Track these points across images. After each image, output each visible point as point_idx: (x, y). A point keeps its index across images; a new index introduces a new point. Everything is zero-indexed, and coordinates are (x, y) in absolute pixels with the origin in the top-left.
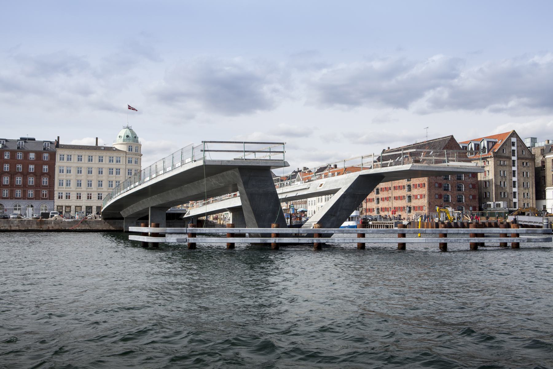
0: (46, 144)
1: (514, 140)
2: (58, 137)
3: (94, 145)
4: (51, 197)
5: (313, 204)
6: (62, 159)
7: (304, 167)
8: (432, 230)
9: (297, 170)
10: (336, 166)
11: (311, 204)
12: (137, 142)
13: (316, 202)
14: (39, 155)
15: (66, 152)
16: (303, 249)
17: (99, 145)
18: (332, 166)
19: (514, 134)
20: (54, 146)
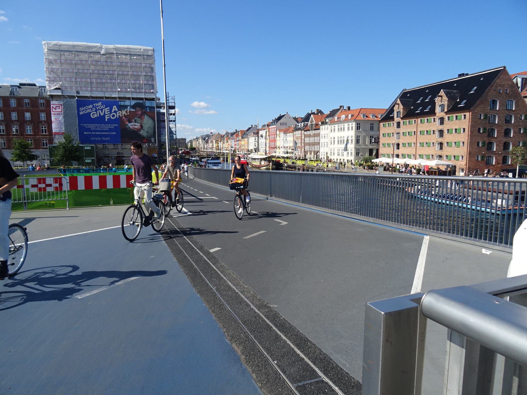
0: (42, 89)
5: (326, 146)
7: (317, 110)
8: (56, 194)
9: (310, 112)
10: (349, 108)
11: (323, 145)
13: (328, 144)
18: (345, 108)
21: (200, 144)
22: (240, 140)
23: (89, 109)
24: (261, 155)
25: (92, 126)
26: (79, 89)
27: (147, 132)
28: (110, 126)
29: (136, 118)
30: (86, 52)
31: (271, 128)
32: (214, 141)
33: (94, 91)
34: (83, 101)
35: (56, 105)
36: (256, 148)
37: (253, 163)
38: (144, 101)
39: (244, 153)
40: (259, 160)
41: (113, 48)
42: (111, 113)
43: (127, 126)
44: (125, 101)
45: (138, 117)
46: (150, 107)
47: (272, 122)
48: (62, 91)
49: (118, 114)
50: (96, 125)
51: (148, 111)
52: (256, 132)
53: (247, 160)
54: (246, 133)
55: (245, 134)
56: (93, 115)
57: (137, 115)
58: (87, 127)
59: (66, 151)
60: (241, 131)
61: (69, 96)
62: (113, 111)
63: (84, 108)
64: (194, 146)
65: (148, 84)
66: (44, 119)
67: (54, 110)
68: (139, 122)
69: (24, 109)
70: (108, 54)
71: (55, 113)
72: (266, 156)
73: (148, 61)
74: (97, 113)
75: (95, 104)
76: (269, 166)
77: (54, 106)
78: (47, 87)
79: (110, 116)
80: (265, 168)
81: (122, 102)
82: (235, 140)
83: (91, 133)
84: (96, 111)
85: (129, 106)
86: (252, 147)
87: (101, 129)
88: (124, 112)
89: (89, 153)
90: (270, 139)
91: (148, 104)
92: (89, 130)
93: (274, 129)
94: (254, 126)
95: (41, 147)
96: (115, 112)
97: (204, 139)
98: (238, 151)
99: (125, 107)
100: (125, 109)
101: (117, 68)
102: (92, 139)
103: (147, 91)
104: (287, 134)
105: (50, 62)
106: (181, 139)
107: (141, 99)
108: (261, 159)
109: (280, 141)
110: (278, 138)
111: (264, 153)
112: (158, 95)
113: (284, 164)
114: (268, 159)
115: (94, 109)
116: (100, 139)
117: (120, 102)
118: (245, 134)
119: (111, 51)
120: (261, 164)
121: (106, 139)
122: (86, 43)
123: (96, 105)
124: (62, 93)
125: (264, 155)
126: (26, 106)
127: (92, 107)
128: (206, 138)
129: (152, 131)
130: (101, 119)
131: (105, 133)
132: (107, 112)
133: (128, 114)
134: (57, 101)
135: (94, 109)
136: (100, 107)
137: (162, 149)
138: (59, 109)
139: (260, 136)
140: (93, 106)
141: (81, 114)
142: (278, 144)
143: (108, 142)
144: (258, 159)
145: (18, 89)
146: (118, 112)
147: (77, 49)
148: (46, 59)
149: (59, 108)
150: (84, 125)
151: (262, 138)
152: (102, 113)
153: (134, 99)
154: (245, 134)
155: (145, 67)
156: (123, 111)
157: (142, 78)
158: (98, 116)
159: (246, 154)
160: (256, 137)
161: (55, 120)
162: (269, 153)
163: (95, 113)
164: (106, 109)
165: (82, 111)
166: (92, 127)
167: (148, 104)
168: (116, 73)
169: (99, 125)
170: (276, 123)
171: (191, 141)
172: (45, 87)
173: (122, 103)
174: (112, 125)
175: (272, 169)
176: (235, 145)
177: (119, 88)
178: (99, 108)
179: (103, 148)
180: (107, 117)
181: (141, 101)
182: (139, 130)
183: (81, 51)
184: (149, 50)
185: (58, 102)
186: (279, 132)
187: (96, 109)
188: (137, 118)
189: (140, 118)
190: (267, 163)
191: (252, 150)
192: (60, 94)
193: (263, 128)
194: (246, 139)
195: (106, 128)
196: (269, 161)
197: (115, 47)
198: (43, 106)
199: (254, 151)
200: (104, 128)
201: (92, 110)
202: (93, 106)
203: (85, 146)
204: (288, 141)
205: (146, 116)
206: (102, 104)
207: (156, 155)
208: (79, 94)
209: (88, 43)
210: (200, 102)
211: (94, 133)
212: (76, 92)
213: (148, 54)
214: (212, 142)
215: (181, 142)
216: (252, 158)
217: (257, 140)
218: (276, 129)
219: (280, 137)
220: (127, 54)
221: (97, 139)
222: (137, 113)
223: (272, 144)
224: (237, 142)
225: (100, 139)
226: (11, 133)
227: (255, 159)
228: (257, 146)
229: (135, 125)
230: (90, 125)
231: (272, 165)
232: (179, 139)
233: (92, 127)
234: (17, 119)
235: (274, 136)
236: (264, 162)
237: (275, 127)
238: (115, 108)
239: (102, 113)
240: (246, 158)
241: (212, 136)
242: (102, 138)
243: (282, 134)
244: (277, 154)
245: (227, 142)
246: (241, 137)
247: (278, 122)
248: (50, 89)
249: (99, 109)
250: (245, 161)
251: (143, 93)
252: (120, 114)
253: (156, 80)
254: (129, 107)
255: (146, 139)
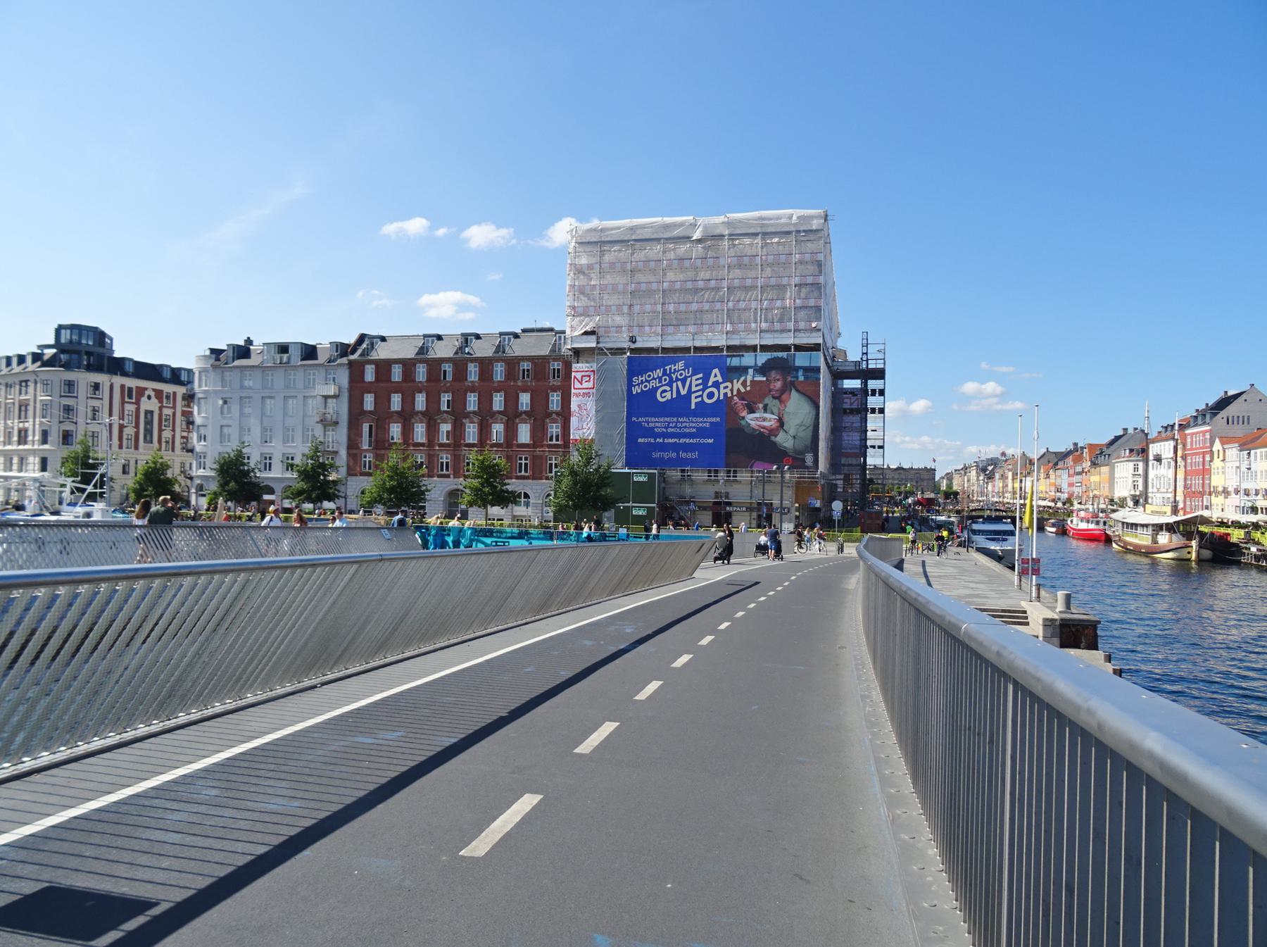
21: (971, 484)
22: (1086, 470)
23: (654, 379)
24: (1158, 512)
25: (657, 423)
26: (635, 332)
27: (794, 437)
28: (701, 422)
29: (768, 400)
30: (658, 240)
31: (1192, 434)
32: (1010, 475)
33: (670, 334)
34: (641, 361)
35: (583, 374)
36: (1138, 493)
37: (1128, 539)
38: (792, 352)
39: (1095, 507)
40: (1150, 528)
41: (723, 223)
42: (706, 387)
43: (743, 423)
44: (743, 356)
45: (774, 398)
46: (806, 369)
47: (1196, 417)
48: (598, 338)
49: (722, 391)
50: (668, 419)
51: (801, 378)
52: (1137, 447)
53: (1107, 527)
54: (1107, 451)
55: (1101, 454)
56: (663, 395)
57: (770, 391)
58: (646, 425)
59: (575, 484)
60: (1091, 446)
61: (611, 349)
62: (710, 384)
63: (644, 378)
64: (955, 488)
65: (806, 307)
66: (557, 407)
67: (577, 385)
68: (776, 411)
69: (519, 384)
70: (712, 238)
71: (579, 391)
72: (1174, 519)
73: (810, 246)
74: (672, 390)
75: (668, 368)
76: (1189, 549)
77: (579, 376)
78: (568, 332)
79: (701, 396)
80: (1170, 555)
81: (734, 358)
82: (1072, 472)
83: (655, 440)
84: (670, 384)
85: (751, 367)
86: (1123, 490)
87: (678, 430)
88: (737, 385)
89: (643, 492)
90: (1189, 468)
91: (801, 360)
92: (650, 432)
93: (1204, 436)
94: (1131, 431)
95: (544, 474)
96: (716, 385)
97: (984, 470)
98: (1080, 503)
99: (743, 370)
100: (741, 376)
101: (729, 272)
102: (656, 455)
103: (802, 325)
104: (1252, 452)
105: (579, 271)
106: (922, 469)
107: (785, 348)
108: (1159, 528)
109: (1224, 473)
110: (1217, 463)
111: (1168, 509)
112: (841, 344)
113: (1248, 546)
114: (1186, 529)
115: (665, 380)
116: (674, 455)
117: (729, 360)
118: (1102, 453)
119: (718, 232)
120: (1155, 541)
121: (689, 455)
122: (660, 219)
123: (670, 369)
124: (598, 343)
125: (1169, 513)
126: (524, 378)
127: (660, 375)
128: (988, 469)
129: (807, 435)
130: (679, 406)
131: (687, 441)
132: (697, 386)
133: (748, 388)
134: (587, 362)
135: (665, 380)
136: (681, 375)
137: (869, 492)
138: (589, 381)
139: (1151, 457)
140: (665, 371)
141: (634, 393)
142: (1217, 481)
143: (692, 462)
144: (1146, 526)
145: (512, 339)
146: (722, 386)
147: (646, 234)
148: (571, 264)
149: (588, 379)
150: (640, 419)
151: (1160, 464)
152: (684, 388)
153: (765, 348)
154: (1101, 454)
155: (801, 262)
156: (735, 381)
157: (791, 292)
158: (674, 396)
159: (1103, 511)
160: (1137, 461)
161: (577, 409)
162: (1184, 508)
163: (668, 388)
164: (694, 378)
165: (638, 384)
166: (657, 424)
167: (801, 360)
168: (725, 284)
169: (675, 419)
170: (1211, 419)
171: (949, 477)
172: (564, 332)
173: (735, 362)
174: (705, 420)
176: (1071, 485)
178: (677, 377)
179: (683, 479)
180: (696, 397)
181: (784, 354)
182: (774, 432)
183: (647, 237)
184: (812, 217)
185: (587, 365)
186: (1223, 443)
187: (671, 378)
188: (771, 399)
189: (778, 398)
190: (1177, 540)
191: (1125, 499)
192: (594, 345)
193: (1163, 435)
194: (1105, 469)
195: (691, 427)
196: (1189, 536)
197: (726, 219)
198: (558, 377)
199: (1130, 503)
200: (685, 427)
201: (660, 382)
202: (665, 371)
203: (634, 473)
204: (1259, 474)
205: (794, 393)
206: (686, 367)
207: (819, 501)
208: (634, 342)
209: (665, 219)
210: (983, 382)
211: (661, 441)
212: (628, 339)
213: (810, 228)
214: (1003, 477)
215: (922, 477)
216: (1123, 523)
217: (1141, 471)
218: (1211, 437)
219: (1224, 460)
220: (756, 234)
221: (666, 455)
222: (772, 387)
223: (1196, 483)
224: (1078, 478)
225: (674, 455)
226: (488, 442)
227: (1136, 525)
228: (1141, 488)
229: (764, 420)
230: (653, 419)
231: (1200, 546)
232: (919, 469)
233: (657, 424)
234: (502, 409)
235: (1204, 458)
236: (1167, 537)
237: (1206, 431)
238: (716, 375)
239: (684, 388)
240: (1102, 524)
241: (1006, 461)
242: (678, 454)
243: (1233, 452)
244: (1215, 515)
245: (1048, 476)
246: (1089, 463)
247: (1219, 416)
248: (573, 330)
249: (677, 380)
250: (1100, 530)
251: (790, 331)
252: (728, 391)
253: (834, 300)
254: (751, 371)
255: (790, 456)
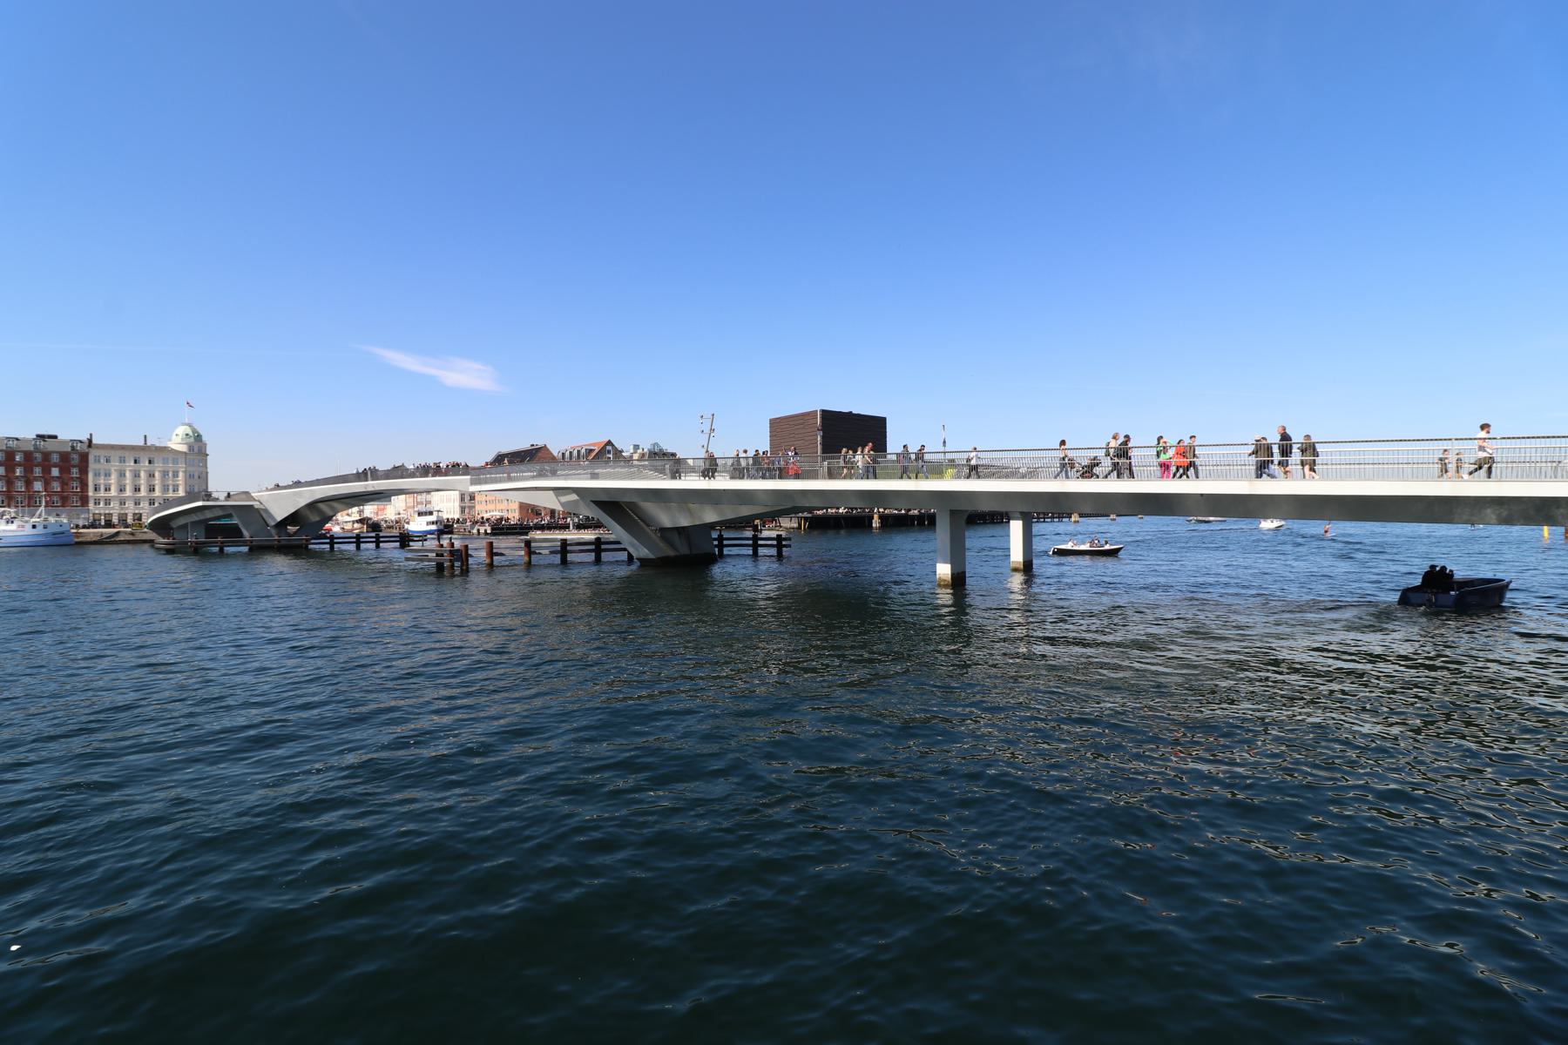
1: (609, 448)
2: (91, 435)
3: (142, 443)
4: (84, 501)
6: (97, 460)
12: (201, 441)
14: (65, 457)
15: (102, 453)
16: (463, 805)
17: (149, 444)
19: (609, 443)
20: (85, 447)
108: (354, 522)
114: (361, 521)
175: (367, 532)
177: (1358, 937)
